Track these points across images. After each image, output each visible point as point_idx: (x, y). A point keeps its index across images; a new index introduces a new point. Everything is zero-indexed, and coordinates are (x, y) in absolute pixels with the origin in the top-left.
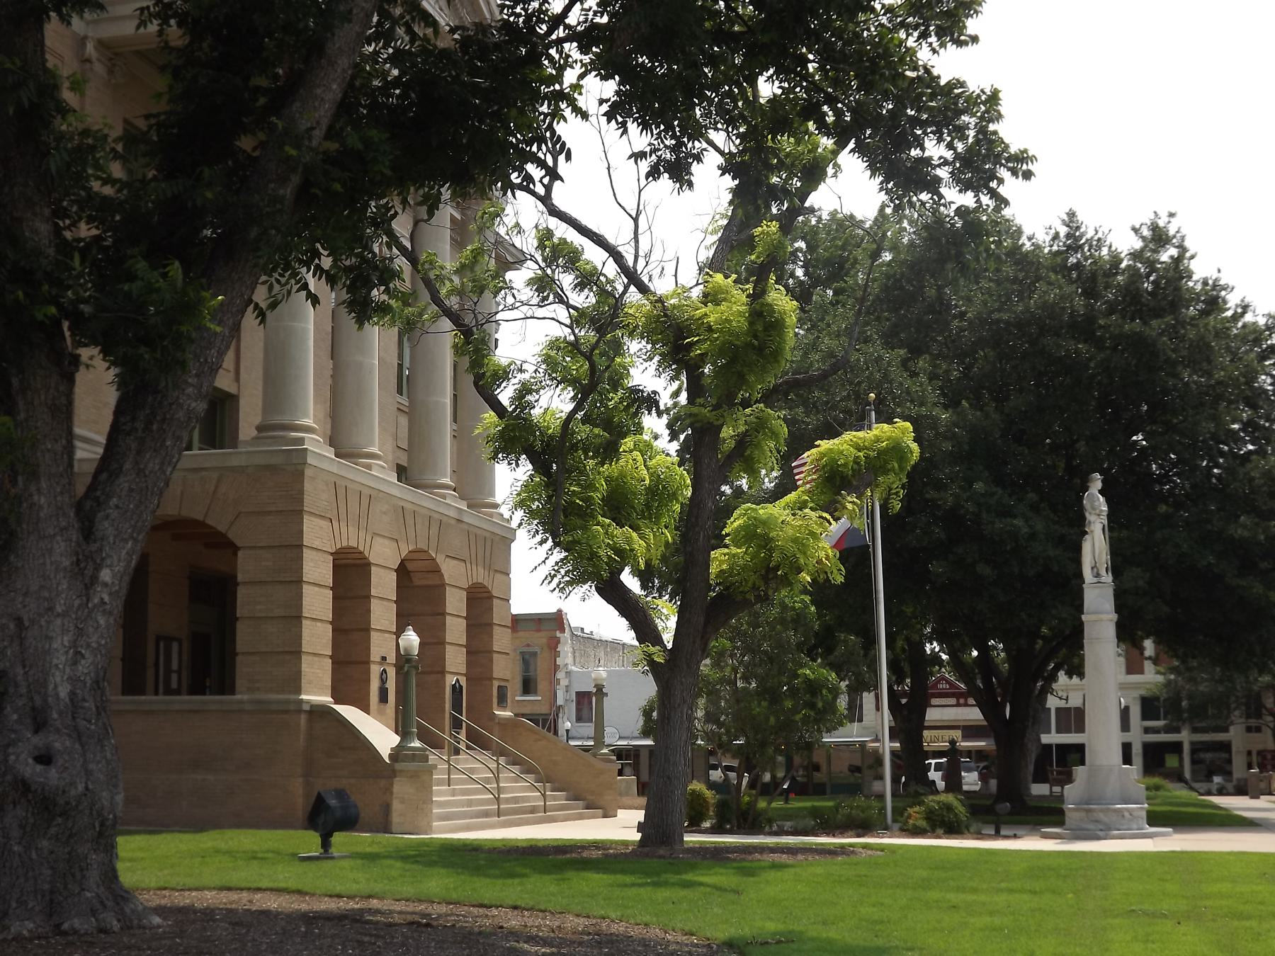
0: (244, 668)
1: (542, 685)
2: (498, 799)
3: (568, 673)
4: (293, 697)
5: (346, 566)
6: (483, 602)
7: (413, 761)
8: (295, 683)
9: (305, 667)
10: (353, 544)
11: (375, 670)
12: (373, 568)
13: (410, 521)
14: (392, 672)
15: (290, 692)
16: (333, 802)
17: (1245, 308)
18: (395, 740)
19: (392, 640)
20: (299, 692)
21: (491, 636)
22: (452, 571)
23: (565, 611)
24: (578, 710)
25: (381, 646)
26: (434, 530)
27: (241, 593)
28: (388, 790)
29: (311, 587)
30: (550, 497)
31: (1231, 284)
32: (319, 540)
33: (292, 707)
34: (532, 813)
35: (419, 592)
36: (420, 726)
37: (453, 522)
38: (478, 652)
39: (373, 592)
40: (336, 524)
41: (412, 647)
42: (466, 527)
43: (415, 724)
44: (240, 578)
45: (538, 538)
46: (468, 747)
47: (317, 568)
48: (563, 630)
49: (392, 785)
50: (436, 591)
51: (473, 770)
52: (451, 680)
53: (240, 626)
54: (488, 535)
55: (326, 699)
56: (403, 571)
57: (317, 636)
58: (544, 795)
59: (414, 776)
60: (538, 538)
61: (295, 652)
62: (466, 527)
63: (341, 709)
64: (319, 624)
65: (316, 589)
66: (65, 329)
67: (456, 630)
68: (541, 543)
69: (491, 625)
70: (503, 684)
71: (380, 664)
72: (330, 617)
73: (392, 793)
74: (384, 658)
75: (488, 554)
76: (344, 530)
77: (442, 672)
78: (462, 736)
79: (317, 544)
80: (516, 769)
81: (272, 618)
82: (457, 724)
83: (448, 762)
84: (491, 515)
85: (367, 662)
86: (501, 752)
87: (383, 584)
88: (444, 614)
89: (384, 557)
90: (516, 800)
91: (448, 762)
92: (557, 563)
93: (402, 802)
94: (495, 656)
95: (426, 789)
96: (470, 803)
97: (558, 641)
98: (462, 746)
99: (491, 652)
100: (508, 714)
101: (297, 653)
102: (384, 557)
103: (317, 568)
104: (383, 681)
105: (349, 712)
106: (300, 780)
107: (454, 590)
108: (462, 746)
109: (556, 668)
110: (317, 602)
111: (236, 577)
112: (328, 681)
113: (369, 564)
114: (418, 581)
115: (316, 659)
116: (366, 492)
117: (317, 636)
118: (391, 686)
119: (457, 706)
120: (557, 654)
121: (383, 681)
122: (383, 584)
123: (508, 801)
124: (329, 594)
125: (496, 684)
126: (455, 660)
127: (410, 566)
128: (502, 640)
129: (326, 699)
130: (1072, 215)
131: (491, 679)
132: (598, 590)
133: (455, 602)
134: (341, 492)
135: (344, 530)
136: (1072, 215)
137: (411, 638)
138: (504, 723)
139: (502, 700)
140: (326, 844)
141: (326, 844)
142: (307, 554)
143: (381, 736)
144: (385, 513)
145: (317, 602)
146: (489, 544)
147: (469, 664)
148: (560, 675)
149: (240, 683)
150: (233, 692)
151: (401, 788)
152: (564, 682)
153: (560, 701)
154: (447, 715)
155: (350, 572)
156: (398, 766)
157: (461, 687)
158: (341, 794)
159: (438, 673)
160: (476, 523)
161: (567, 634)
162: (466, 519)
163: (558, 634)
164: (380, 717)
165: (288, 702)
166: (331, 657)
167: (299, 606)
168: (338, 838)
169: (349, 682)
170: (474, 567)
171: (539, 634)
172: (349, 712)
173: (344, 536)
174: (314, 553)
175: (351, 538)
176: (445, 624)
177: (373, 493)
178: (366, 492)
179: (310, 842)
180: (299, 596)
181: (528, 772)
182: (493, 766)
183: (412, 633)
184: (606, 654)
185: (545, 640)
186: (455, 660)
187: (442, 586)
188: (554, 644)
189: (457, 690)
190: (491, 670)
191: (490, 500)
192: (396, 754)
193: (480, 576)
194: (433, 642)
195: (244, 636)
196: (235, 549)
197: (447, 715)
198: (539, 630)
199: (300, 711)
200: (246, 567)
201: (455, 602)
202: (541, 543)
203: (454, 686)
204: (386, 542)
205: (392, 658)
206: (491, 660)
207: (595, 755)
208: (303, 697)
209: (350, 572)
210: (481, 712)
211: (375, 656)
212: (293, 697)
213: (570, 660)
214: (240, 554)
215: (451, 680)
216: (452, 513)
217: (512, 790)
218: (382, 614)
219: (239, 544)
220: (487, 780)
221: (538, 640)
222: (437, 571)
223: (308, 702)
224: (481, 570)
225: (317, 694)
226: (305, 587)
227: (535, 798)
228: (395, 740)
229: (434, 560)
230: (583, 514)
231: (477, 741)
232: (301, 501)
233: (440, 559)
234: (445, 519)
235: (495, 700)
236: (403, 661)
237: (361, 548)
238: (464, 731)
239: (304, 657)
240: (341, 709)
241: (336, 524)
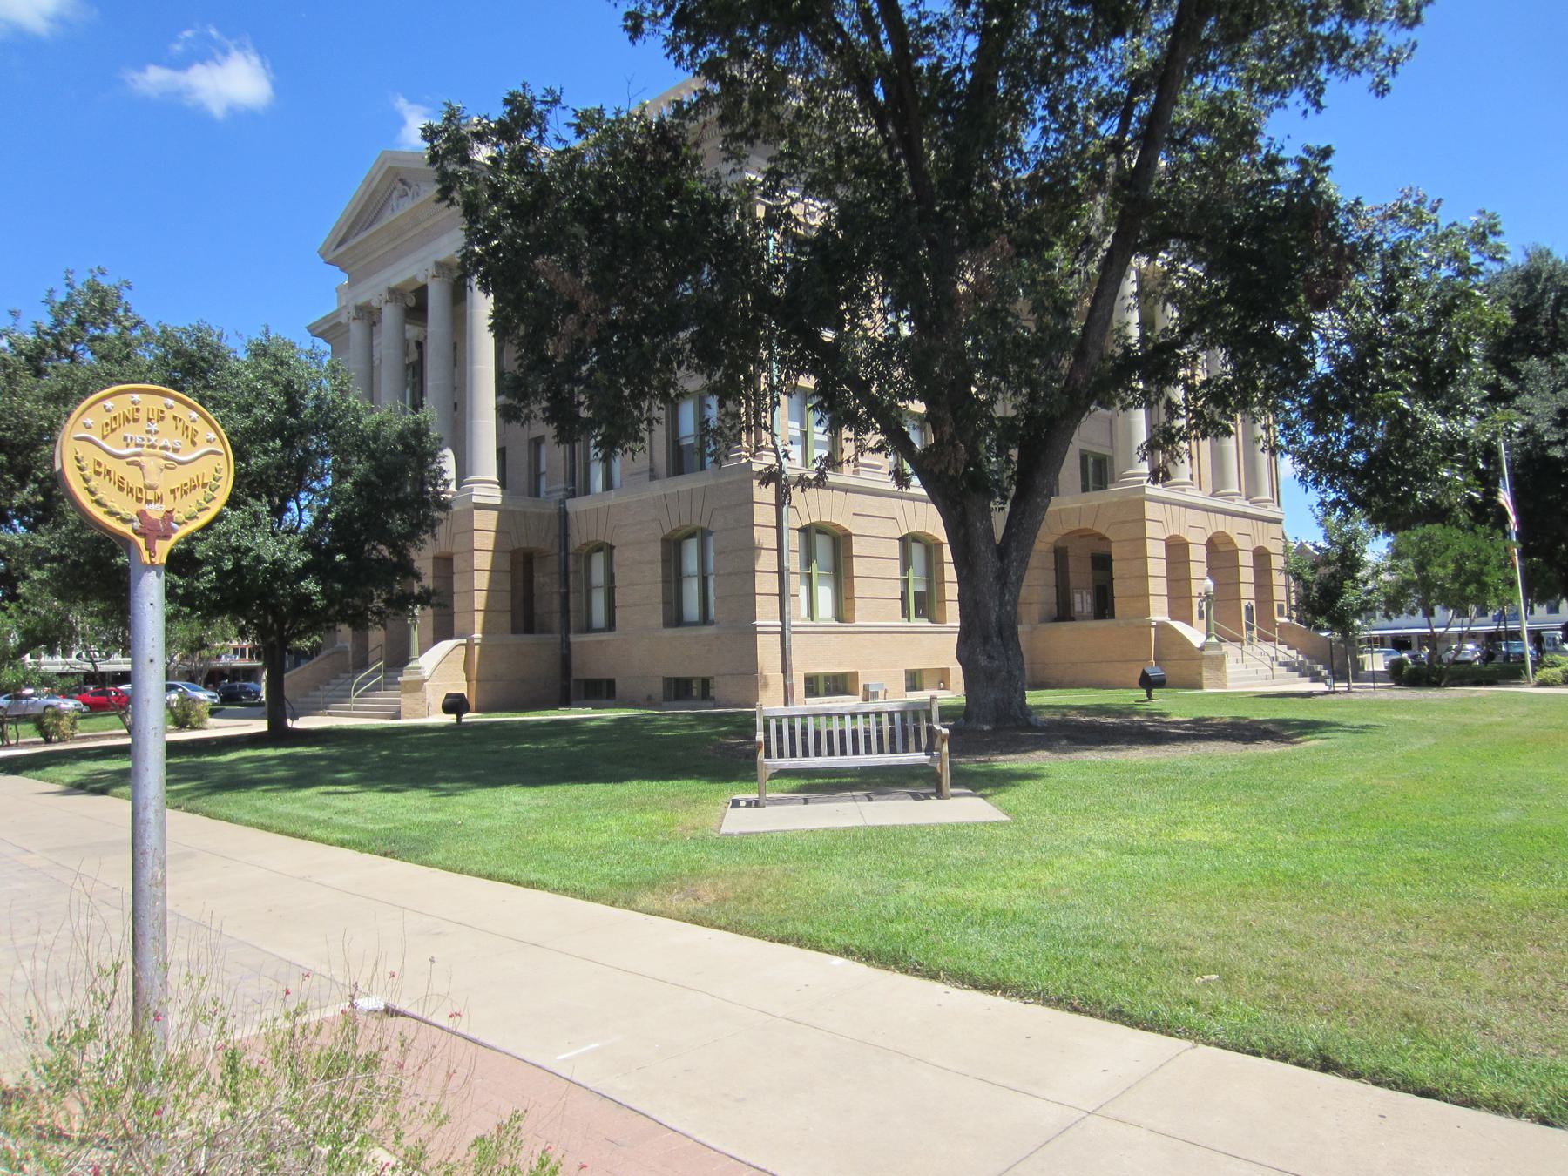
11: (1195, 601)
17: (668, 56)
19: (1201, 583)
31: (639, 42)
50: (1234, 553)
52: (1244, 603)
55: (1166, 619)
57: (1158, 586)
66: (1513, 518)
82: (1250, 628)
87: (1198, 554)
101: (1147, 595)
103: (1156, 549)
105: (1179, 626)
110: (1157, 567)
117: (1158, 586)
119: (1250, 618)
122: (1198, 554)
129: (1166, 619)
130: (1326, 153)
133: (1245, 559)
136: (1326, 153)
140: (1149, 695)
141: (1149, 695)
143: (1195, 635)
145: (1157, 567)
155: (1177, 550)
168: (1155, 692)
172: (1179, 626)
179: (1143, 694)
187: (1237, 550)
189: (1249, 609)
201: (1245, 559)
209: (1177, 550)
222: (1232, 542)
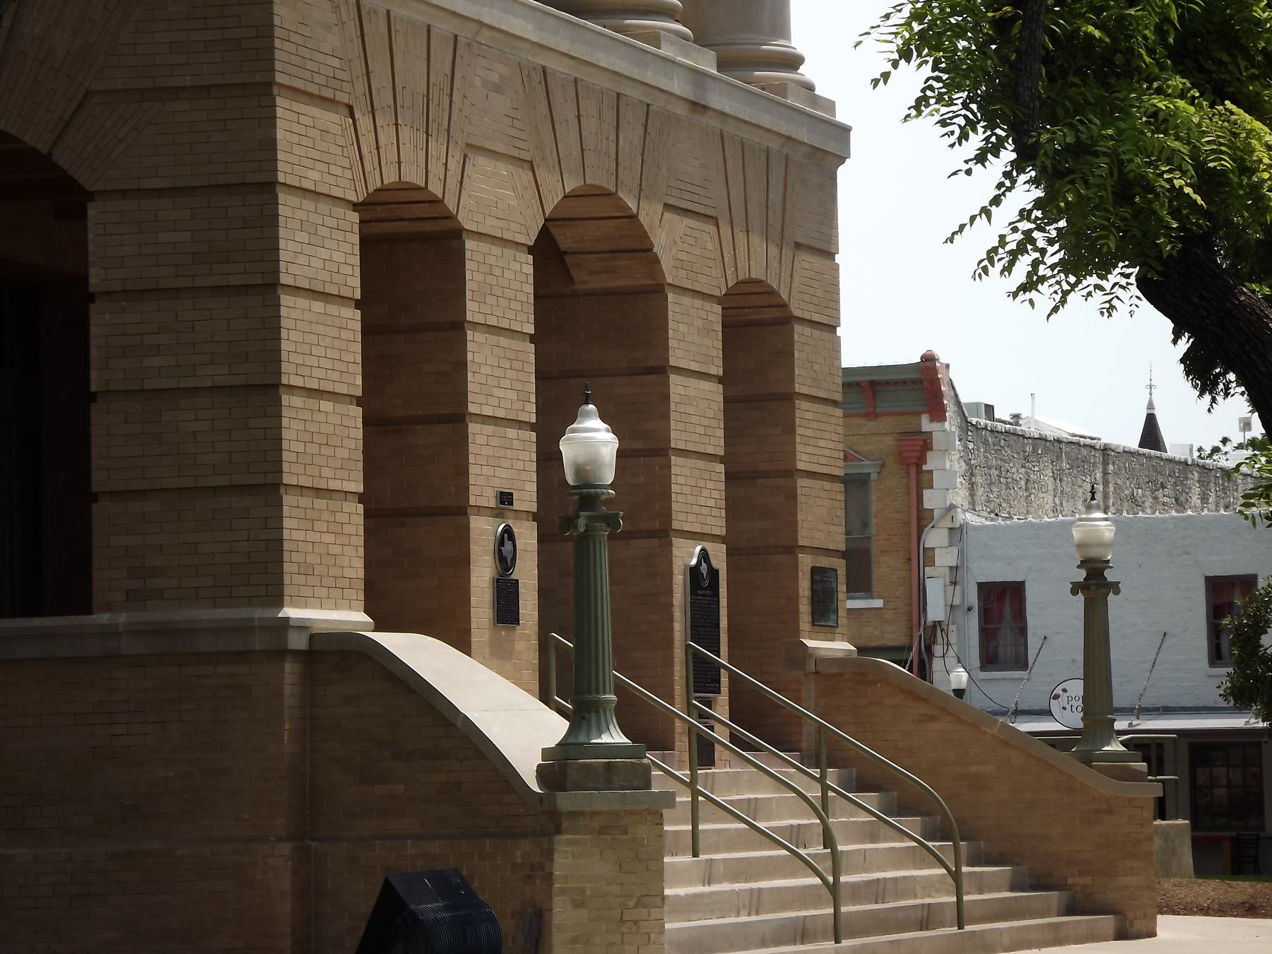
0: (114, 535)
1: (885, 568)
2: (834, 889)
3: (958, 533)
4: (258, 613)
5: (391, 239)
6: (768, 331)
7: (609, 785)
8: (265, 575)
9: (292, 530)
10: (413, 176)
11: (483, 530)
12: (470, 244)
13: (565, 110)
14: (527, 537)
15: (250, 601)
16: (430, 908)
18: (553, 728)
20: (277, 599)
21: (790, 430)
22: (676, 245)
23: (943, 359)
24: (987, 634)
25: (498, 463)
26: (631, 137)
27: (102, 323)
28: (541, 871)
29: (302, 302)
30: (1002, 26)
32: (321, 163)
33: (258, 643)
34: (923, 925)
35: (595, 317)
36: (620, 689)
37: (681, 110)
38: (757, 475)
39: (473, 311)
40: (364, 122)
41: (595, 462)
42: (715, 123)
43: (610, 684)
44: (96, 279)
45: (976, 141)
46: (734, 738)
47: (318, 252)
48: (938, 413)
49: (549, 854)
50: (642, 303)
51: (754, 807)
52: (687, 554)
53: (100, 418)
54: (775, 144)
55: (352, 617)
56: (548, 252)
57: (322, 441)
58: (956, 876)
59: (609, 827)
60: (976, 141)
61: (266, 487)
62: (715, 123)
63: (387, 640)
64: (326, 406)
65: (318, 306)
67: (696, 412)
68: (981, 158)
69: (789, 397)
70: (824, 562)
71: (498, 513)
72: (356, 384)
73: (549, 878)
74: (505, 498)
75: (776, 195)
76: (387, 136)
77: (664, 533)
78: (721, 710)
79: (312, 178)
80: (869, 800)
81: (195, 391)
82: (704, 677)
83: (692, 785)
84: (781, 89)
85: (461, 511)
86: (822, 754)
87: (499, 289)
88: (662, 370)
89: (498, 207)
90: (876, 890)
91: (692, 785)
92: (1024, 215)
93: (578, 905)
94: (802, 482)
95: (644, 867)
96: (756, 901)
97: (925, 444)
98: (720, 735)
99: (791, 473)
100: (840, 646)
102: (498, 207)
103: (318, 252)
104: (505, 562)
105: (418, 652)
106: (286, 848)
107: (687, 300)
108: (720, 735)
109: (923, 519)
110: (321, 345)
111: (85, 278)
112: (355, 567)
113: (454, 236)
114: (586, 279)
115: (321, 503)
116: (443, 27)
117: (322, 441)
118: (527, 573)
119: (703, 627)
120: (922, 480)
121: (505, 562)
122: (499, 289)
123: (858, 892)
124: (353, 318)
125: (806, 562)
126: (698, 500)
127: (566, 238)
128: (818, 441)
129: (352, 617)
131: (792, 549)
132: (1143, 284)
133: (693, 337)
134: (376, 29)
135: (387, 136)
137: (593, 440)
138: (832, 675)
139: (823, 611)
142: (288, 207)
143: (519, 725)
144: (498, 89)
145: (321, 345)
146: (777, 172)
147: (733, 508)
148: (935, 538)
149: (106, 577)
150: (86, 608)
151: (573, 861)
152: (945, 558)
153: (936, 611)
154: (679, 654)
155: (409, 254)
156: (566, 801)
157: (714, 573)
158: (451, 887)
159: (651, 534)
160: (745, 112)
161: (951, 424)
162: (716, 101)
163: (926, 424)
164: (499, 658)
165: (244, 628)
166: (362, 498)
167: (272, 358)
169: (414, 571)
170: (741, 237)
171: (870, 426)
172: (418, 652)
173: (389, 155)
174: (308, 204)
175: (407, 160)
176: (666, 398)
177: (466, 33)
178: (443, 27)
180: (271, 327)
181: (902, 809)
182: (814, 793)
183: (596, 423)
184: (1058, 477)
185: (889, 442)
186: (698, 500)
187: (656, 291)
188: (915, 451)
190: (793, 526)
191: (775, 46)
192: (557, 766)
193: (758, 260)
194: (645, 449)
195: (114, 445)
196: (70, 201)
197: (679, 654)
198: (872, 415)
199: (281, 653)
200: (114, 247)
201: (693, 337)
202: (981, 158)
203: (694, 571)
204: (503, 169)
205: (527, 499)
206: (792, 497)
207: (1087, 759)
208: (291, 612)
209: (409, 254)
210: (770, 644)
211: (481, 492)
212: (258, 613)
213: (959, 497)
214: (93, 211)
215: (687, 554)
216: (679, 86)
217: (865, 861)
218: (499, 375)
219: (87, 180)
220: (797, 834)
221: (880, 438)
222: (641, 249)
223: (303, 626)
224: (757, 243)
225: (326, 608)
226: (286, 300)
227: (930, 885)
228: (553, 728)
229: (633, 217)
230: (1112, 68)
231: (762, 725)
232: (266, 56)
233: (649, 214)
234: (659, 102)
235: (805, 608)
236: (567, 507)
237: (435, 188)
238: (723, 699)
239: (288, 500)
240: (387, 640)
241: (364, 122)
